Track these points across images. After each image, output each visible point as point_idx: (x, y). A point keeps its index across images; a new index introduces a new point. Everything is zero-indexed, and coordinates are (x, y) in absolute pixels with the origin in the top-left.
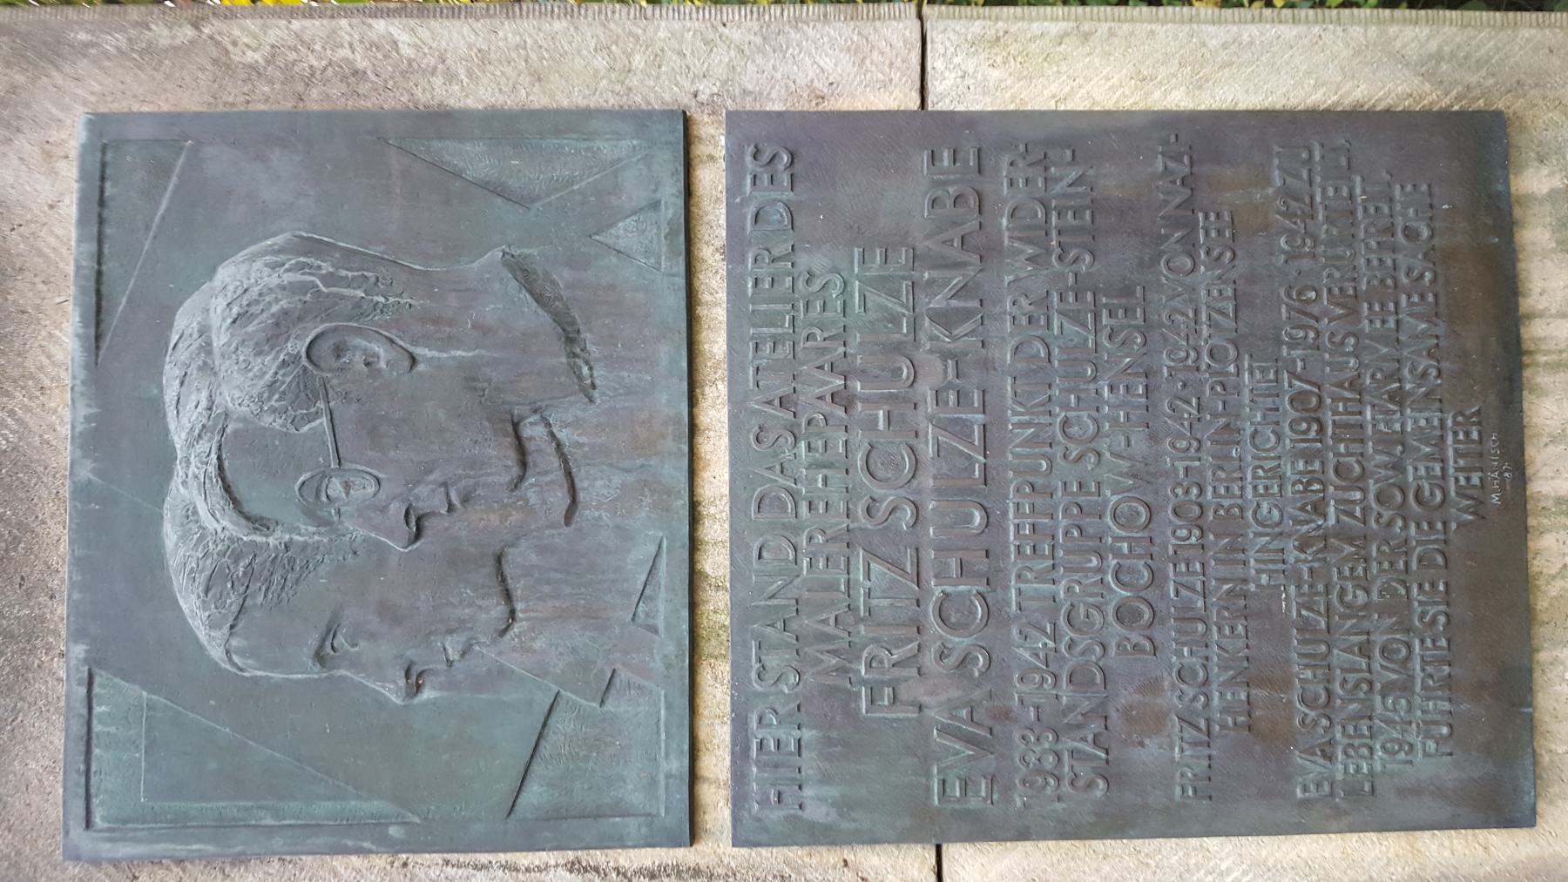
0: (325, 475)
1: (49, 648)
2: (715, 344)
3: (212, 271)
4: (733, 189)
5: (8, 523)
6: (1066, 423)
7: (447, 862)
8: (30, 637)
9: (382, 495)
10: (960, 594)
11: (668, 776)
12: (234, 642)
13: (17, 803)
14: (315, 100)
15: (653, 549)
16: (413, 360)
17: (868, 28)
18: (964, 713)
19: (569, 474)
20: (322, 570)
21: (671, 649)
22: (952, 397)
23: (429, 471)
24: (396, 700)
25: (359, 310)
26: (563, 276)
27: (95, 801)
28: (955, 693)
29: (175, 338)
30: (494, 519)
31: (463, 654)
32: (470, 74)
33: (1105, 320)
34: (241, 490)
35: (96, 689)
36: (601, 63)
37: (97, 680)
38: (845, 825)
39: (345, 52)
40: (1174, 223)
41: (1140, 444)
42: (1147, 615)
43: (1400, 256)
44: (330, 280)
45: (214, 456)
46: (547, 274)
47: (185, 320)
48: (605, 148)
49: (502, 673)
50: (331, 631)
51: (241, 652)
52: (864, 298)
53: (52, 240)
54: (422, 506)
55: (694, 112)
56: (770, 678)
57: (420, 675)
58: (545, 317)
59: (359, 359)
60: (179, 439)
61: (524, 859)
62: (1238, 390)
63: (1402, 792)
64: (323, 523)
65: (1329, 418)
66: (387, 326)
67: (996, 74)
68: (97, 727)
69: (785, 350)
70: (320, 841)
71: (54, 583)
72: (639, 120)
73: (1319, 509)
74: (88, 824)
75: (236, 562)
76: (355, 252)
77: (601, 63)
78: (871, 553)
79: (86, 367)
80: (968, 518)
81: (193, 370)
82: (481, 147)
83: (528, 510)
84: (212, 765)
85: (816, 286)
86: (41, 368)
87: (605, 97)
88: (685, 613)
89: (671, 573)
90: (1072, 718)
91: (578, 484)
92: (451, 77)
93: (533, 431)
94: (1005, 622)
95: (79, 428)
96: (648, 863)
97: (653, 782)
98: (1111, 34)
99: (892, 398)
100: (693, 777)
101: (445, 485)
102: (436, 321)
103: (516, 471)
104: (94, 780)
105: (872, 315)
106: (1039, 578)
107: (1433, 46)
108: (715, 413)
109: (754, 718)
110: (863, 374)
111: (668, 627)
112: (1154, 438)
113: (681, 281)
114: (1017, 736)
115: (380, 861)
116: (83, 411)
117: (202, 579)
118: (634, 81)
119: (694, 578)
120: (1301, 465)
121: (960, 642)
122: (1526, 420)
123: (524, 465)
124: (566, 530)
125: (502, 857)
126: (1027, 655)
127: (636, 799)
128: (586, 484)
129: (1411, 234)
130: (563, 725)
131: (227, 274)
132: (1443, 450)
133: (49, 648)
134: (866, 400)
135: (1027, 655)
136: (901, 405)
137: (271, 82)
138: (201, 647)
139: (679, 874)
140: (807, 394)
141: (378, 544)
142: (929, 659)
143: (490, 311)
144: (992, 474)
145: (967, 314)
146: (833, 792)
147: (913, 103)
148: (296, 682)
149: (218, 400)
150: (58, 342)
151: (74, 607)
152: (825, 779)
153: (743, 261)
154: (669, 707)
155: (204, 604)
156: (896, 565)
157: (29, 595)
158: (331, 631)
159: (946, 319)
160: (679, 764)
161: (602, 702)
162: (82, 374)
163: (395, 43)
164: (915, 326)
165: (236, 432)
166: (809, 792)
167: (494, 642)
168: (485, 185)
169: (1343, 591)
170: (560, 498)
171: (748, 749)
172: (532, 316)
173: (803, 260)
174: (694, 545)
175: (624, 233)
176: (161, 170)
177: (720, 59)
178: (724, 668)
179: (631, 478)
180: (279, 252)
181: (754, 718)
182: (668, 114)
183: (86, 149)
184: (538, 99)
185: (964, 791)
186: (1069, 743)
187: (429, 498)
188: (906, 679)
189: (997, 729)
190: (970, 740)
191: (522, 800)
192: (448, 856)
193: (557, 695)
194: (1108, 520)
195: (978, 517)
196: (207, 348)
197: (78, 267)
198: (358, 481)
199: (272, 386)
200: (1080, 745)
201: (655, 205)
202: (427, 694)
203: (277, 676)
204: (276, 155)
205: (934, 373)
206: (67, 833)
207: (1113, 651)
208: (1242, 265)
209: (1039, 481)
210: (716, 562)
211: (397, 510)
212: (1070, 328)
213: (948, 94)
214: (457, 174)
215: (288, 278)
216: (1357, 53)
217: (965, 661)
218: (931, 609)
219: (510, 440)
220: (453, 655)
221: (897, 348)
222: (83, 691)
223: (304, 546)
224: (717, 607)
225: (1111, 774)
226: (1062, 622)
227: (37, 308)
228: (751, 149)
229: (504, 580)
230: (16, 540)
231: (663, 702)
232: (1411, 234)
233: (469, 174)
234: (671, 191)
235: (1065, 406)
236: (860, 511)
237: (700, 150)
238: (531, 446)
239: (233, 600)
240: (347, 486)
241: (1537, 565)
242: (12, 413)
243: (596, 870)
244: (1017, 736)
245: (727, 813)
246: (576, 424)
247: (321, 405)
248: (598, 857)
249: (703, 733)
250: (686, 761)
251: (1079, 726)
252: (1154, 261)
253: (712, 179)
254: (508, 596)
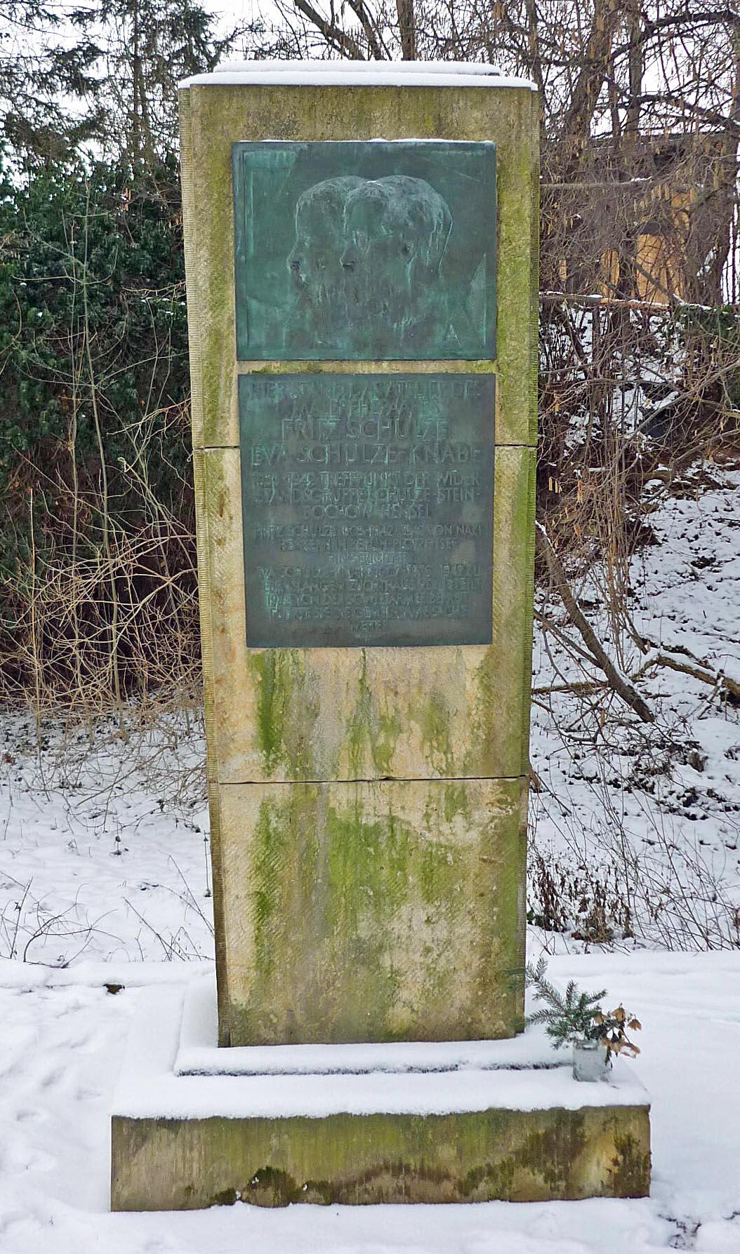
76: (445, 243)
82: (483, 286)
131: (437, 199)
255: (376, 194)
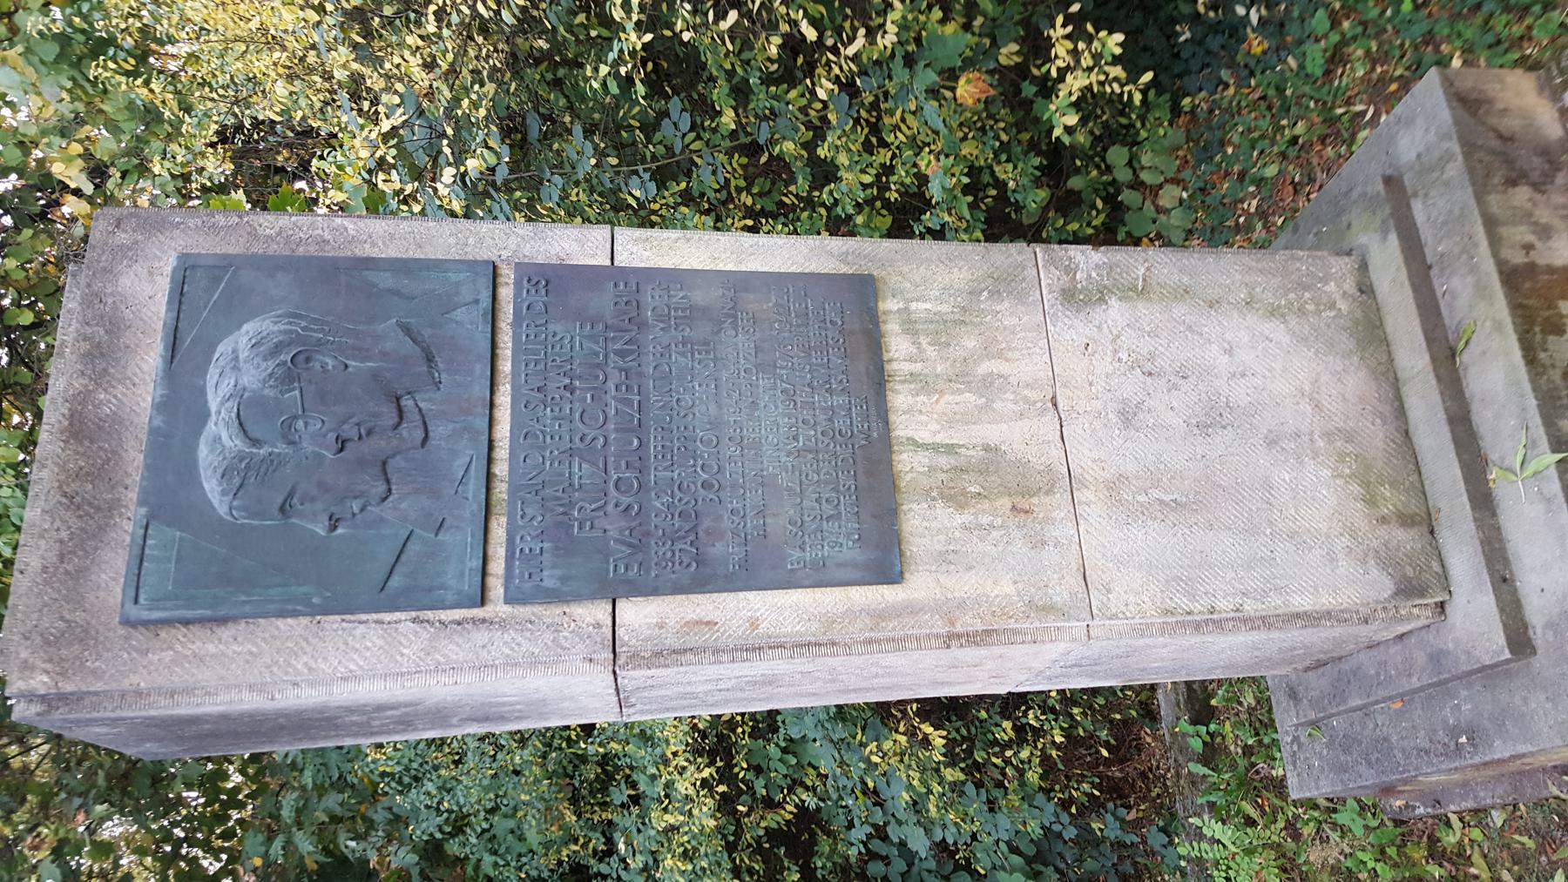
0: (295, 417)
1: (121, 515)
2: (505, 366)
3: (239, 327)
4: (517, 295)
5: (106, 451)
6: (678, 400)
7: (343, 620)
8: (110, 509)
9: (324, 429)
10: (628, 478)
11: (471, 569)
12: (235, 503)
13: (91, 597)
14: (301, 251)
15: (468, 459)
16: (346, 366)
17: (585, 232)
18: (627, 533)
19: (425, 423)
20: (288, 466)
21: (475, 507)
22: (624, 388)
23: (351, 418)
24: (322, 533)
25: (319, 342)
26: (427, 333)
27: (141, 591)
28: (623, 524)
29: (216, 356)
30: (383, 444)
31: (363, 509)
32: (384, 243)
33: (697, 355)
34: (248, 427)
35: (150, 532)
36: (452, 240)
37: (151, 527)
38: (564, 589)
39: (320, 231)
40: (728, 316)
41: (713, 409)
42: (717, 486)
43: (829, 333)
44: (303, 329)
45: (235, 409)
46: (419, 332)
47: (224, 347)
48: (452, 276)
49: (382, 520)
50: (290, 495)
51: (237, 508)
52: (581, 344)
53: (150, 314)
54: (345, 435)
55: (498, 263)
56: (527, 519)
57: (337, 520)
58: (417, 349)
59: (317, 365)
60: (213, 406)
61: (387, 617)
62: (757, 386)
63: (839, 565)
64: (292, 443)
65: (798, 400)
66: (333, 350)
67: (647, 254)
68: (147, 551)
69: (541, 366)
70: (271, 607)
71: (128, 481)
72: (472, 265)
73: (795, 438)
74: (136, 601)
75: (241, 461)
77: (452, 240)
78: (582, 458)
79: (164, 371)
80: (631, 443)
81: (228, 369)
83: (401, 438)
84: (214, 569)
85: (558, 338)
86: (135, 374)
87: (454, 254)
88: (484, 490)
89: (478, 473)
90: (682, 533)
91: (430, 428)
92: (374, 244)
93: (407, 402)
94: (648, 491)
95: (157, 400)
96: (457, 617)
97: (462, 574)
98: (700, 239)
99: (595, 388)
100: (484, 573)
101: (358, 424)
102: (360, 349)
103: (396, 419)
104: (142, 579)
105: (585, 352)
106: (665, 469)
107: (844, 248)
108: (504, 398)
110: (580, 378)
111: (474, 496)
112: (720, 407)
113: (489, 335)
114: (653, 543)
115: (304, 621)
116: (160, 392)
117: (220, 471)
118: (468, 249)
119: (489, 476)
120: (786, 420)
121: (625, 500)
122: (889, 405)
123: (401, 418)
124: (422, 451)
125: (375, 616)
126: (659, 505)
127: (452, 582)
130: (413, 547)
131: (250, 328)
132: (850, 414)
133: (121, 515)
134: (581, 389)
135: (659, 505)
136: (598, 394)
137: (278, 243)
138: (214, 509)
139: (474, 623)
140: (552, 386)
141: (320, 454)
142: (610, 508)
143: (388, 346)
144: (643, 422)
145: (631, 352)
146: (558, 572)
147: (608, 263)
148: (268, 526)
149: (240, 382)
150: (147, 362)
151: (144, 492)
152: (553, 567)
153: (521, 326)
154: (472, 536)
155: (220, 484)
156: (595, 464)
157: (113, 487)
158: (290, 495)
159: (621, 354)
160: (477, 563)
161: (437, 534)
162: (161, 374)
163: (346, 229)
164: (606, 357)
165: (249, 398)
166: (545, 573)
167: (379, 504)
168: (389, 291)
170: (420, 434)
171: (514, 553)
172: (408, 346)
173: (551, 327)
174: (490, 460)
175: (460, 314)
176: (216, 280)
177: (513, 242)
178: (504, 520)
179: (458, 426)
182: (486, 262)
183: (175, 270)
184: (419, 255)
185: (626, 569)
186: (679, 546)
187: (349, 431)
188: (598, 517)
189: (644, 540)
190: (630, 545)
191: (389, 584)
192: (344, 617)
193: (412, 532)
194: (698, 443)
195: (636, 442)
196: (236, 358)
197: (165, 324)
198: (311, 421)
199: (271, 375)
200: (683, 546)
201: (477, 301)
202: (339, 531)
203: (255, 522)
204: (279, 275)
205: (615, 377)
206: (123, 606)
207: (700, 502)
208: (758, 335)
209: (666, 426)
210: (501, 469)
211: (332, 436)
212: (681, 360)
213: (622, 260)
214: (375, 286)
215: (282, 327)
216: (811, 250)
217: (628, 508)
218: (611, 484)
219: (395, 405)
220: (356, 510)
221: (598, 366)
222: (142, 532)
223: (279, 454)
224: (501, 490)
225: (700, 560)
226: (676, 490)
227: (137, 345)
228: (526, 279)
229: (386, 474)
230: (109, 460)
231: (470, 536)
233: (381, 286)
234: (485, 297)
235: (678, 393)
236: (577, 440)
237: (501, 280)
238: (405, 409)
239: (237, 481)
240: (306, 424)
241: (898, 467)
242: (115, 396)
243: (428, 621)
244: (653, 543)
245: (502, 590)
246: (429, 400)
247: (296, 384)
248: (429, 614)
249: (490, 552)
250: (481, 561)
251: (684, 538)
252: (719, 332)
253: (506, 293)
254: (388, 481)
255: (232, 405)
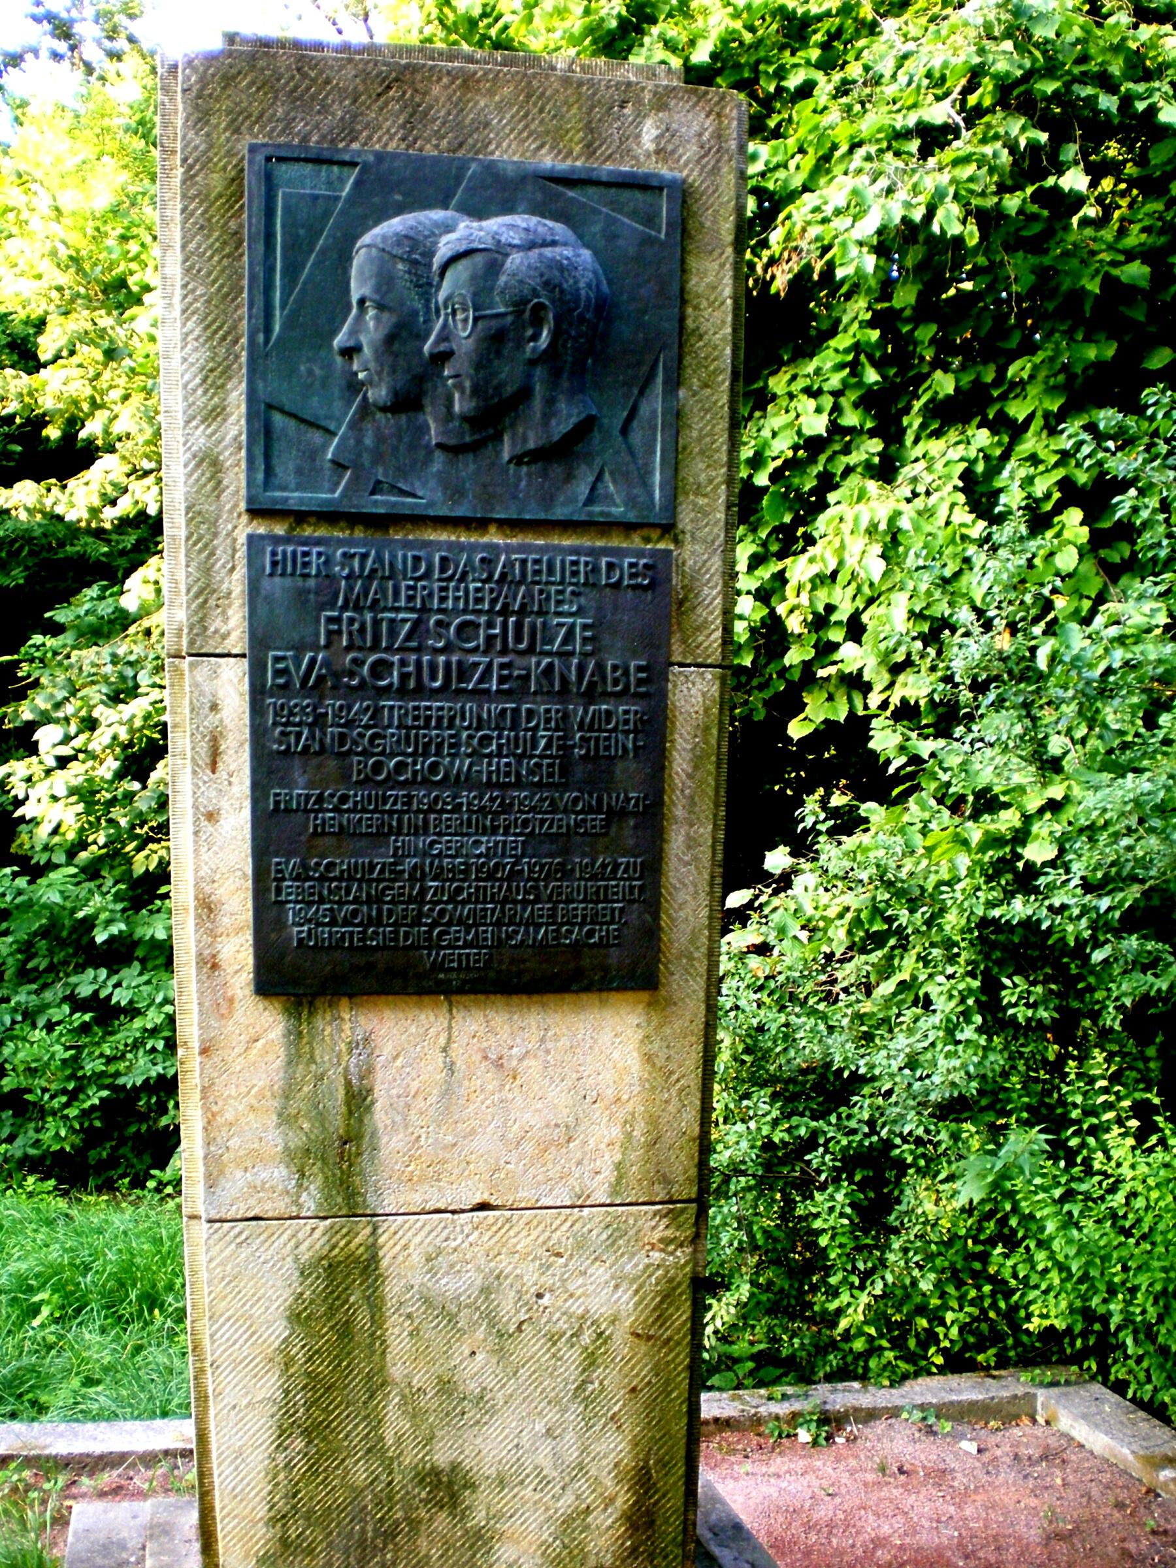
12: (374, 251)
70: (363, 1318)
109: (321, 549)
116: (510, 167)
117: (412, 233)
128: (917, 1388)
129: (590, 934)
152: (283, 589)
169: (392, 889)
171: (304, 544)
180: (598, 286)
181: (321, 549)
215: (583, 292)
232: (590, 934)
